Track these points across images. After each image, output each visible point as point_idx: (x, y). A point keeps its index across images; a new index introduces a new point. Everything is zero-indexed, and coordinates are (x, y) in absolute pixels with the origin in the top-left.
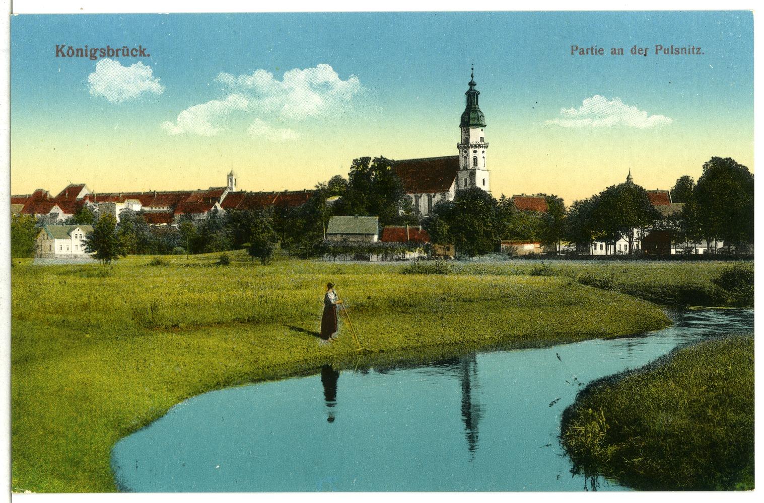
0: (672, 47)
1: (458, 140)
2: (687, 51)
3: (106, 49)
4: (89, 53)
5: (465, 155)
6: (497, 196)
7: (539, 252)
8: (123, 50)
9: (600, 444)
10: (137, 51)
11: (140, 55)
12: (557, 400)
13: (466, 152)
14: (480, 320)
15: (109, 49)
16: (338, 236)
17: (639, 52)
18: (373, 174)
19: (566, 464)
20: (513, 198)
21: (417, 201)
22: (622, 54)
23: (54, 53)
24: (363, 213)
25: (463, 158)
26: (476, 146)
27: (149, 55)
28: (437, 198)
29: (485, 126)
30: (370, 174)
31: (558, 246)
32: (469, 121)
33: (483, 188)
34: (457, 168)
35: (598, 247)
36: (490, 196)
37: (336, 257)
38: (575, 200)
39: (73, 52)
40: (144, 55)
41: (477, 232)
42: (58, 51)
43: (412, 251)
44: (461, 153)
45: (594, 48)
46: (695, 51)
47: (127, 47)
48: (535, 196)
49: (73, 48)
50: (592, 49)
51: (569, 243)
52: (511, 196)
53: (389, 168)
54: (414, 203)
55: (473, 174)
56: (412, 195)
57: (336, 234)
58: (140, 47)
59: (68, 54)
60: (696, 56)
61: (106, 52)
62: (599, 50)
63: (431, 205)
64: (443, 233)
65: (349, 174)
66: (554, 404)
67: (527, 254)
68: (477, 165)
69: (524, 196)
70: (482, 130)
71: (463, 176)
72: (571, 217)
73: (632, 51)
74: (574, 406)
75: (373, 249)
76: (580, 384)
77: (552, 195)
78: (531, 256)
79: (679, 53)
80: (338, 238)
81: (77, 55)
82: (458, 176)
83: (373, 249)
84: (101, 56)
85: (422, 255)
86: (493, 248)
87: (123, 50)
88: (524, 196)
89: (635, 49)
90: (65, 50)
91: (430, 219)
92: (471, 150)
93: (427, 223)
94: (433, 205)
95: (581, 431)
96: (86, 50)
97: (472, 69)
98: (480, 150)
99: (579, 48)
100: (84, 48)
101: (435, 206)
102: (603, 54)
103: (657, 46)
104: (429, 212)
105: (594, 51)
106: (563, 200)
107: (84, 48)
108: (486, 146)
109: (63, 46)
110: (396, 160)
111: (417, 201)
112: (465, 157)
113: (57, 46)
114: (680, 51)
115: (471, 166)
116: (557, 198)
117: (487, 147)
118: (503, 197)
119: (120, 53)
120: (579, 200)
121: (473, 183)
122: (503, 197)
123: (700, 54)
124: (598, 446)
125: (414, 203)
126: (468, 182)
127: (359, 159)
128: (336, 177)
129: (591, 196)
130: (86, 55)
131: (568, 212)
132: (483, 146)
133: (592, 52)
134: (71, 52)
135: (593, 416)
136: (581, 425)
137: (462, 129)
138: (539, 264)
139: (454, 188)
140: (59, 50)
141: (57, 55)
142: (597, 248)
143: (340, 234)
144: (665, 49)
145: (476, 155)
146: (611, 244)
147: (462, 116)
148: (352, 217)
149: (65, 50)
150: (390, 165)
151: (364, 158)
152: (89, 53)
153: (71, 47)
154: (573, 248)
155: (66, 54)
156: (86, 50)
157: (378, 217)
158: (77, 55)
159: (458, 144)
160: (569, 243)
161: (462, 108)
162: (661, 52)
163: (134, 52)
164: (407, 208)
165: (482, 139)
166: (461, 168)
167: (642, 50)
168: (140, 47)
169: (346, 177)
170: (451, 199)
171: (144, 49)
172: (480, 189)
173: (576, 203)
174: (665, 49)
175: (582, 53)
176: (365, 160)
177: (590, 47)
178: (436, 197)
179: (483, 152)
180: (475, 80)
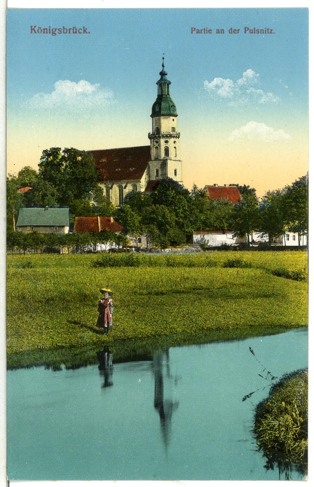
0: (255, 29)
1: (149, 129)
2: (264, 31)
4: (51, 32)
5: (156, 145)
6: (188, 186)
7: (232, 243)
8: (73, 29)
9: (293, 438)
10: (81, 29)
12: (250, 394)
13: (157, 142)
14: (172, 313)
16: (28, 228)
18: (63, 165)
19: (261, 460)
20: (205, 188)
21: (108, 192)
22: (223, 33)
23: (30, 31)
24: (53, 205)
25: (154, 149)
26: (167, 136)
28: (129, 189)
29: (176, 116)
30: (60, 165)
31: (250, 237)
32: (160, 112)
33: (175, 179)
34: (148, 158)
35: (291, 238)
36: (181, 187)
37: (26, 250)
38: (268, 191)
39: (41, 31)
41: (169, 224)
42: (32, 29)
43: (103, 243)
44: (152, 143)
45: (206, 29)
46: (269, 31)
47: (75, 28)
48: (227, 186)
49: (41, 28)
50: (204, 30)
51: (262, 233)
52: (203, 187)
53: (79, 158)
54: (105, 194)
55: (164, 164)
56: (103, 186)
57: (26, 226)
58: (84, 27)
59: (38, 32)
60: (270, 34)
61: (62, 31)
62: (209, 31)
63: (122, 197)
64: (135, 225)
65: (39, 165)
66: (247, 398)
67: (220, 245)
68: (168, 156)
69: (216, 186)
70: (173, 120)
71: (154, 166)
72: (263, 208)
73: (229, 32)
74: (267, 400)
75: (64, 241)
76: (273, 378)
77: (245, 185)
78: (224, 248)
79: (259, 33)
80: (27, 231)
82: (149, 165)
83: (64, 241)
84: (59, 33)
85: (114, 247)
86: (185, 240)
87: (73, 29)
88: (216, 186)
90: (36, 29)
91: (121, 210)
92: (162, 141)
93: (120, 214)
94: (124, 196)
95: (274, 426)
96: (50, 29)
97: (163, 58)
98: (171, 140)
99: (196, 29)
100: (264, 29)
101: (126, 197)
102: (211, 33)
103: (192, 28)
104: (120, 203)
105: (205, 31)
106: (255, 191)
107: (48, 28)
108: (178, 136)
109: (35, 27)
110: (86, 150)
111: (108, 192)
113: (32, 27)
114: (260, 31)
115: (163, 155)
116: (249, 188)
117: (179, 137)
118: (195, 187)
119: (71, 31)
120: (271, 191)
121: (165, 174)
122: (195, 187)
123: (272, 33)
124: (291, 440)
125: (105, 194)
126: (160, 173)
127: (49, 150)
128: (25, 168)
129: (284, 187)
130: (50, 33)
131: (260, 203)
132: (174, 136)
133: (204, 31)
134: (40, 31)
135: (286, 409)
136: (275, 419)
137: (153, 120)
138: (231, 256)
139: (146, 179)
140: (32, 29)
141: (32, 33)
142: (290, 239)
143: (30, 226)
144: (250, 30)
146: (303, 235)
147: (153, 105)
148: (42, 209)
149: (36, 29)
150: (81, 155)
151: (54, 148)
152: (51, 32)
153: (40, 28)
154: (266, 239)
155: (37, 32)
156: (50, 29)
157: (68, 209)
158: (44, 32)
159: (149, 134)
160: (262, 233)
161: (153, 98)
162: (248, 32)
163: (80, 30)
164: (99, 198)
165: (173, 129)
166: (153, 158)
167: (236, 30)
168: (84, 27)
169: (36, 169)
170: (143, 190)
172: (172, 179)
173: (268, 193)
174: (250, 30)
175: (198, 32)
176: (54, 152)
177: (203, 29)
178: (127, 188)
179: (175, 142)
180: (166, 70)
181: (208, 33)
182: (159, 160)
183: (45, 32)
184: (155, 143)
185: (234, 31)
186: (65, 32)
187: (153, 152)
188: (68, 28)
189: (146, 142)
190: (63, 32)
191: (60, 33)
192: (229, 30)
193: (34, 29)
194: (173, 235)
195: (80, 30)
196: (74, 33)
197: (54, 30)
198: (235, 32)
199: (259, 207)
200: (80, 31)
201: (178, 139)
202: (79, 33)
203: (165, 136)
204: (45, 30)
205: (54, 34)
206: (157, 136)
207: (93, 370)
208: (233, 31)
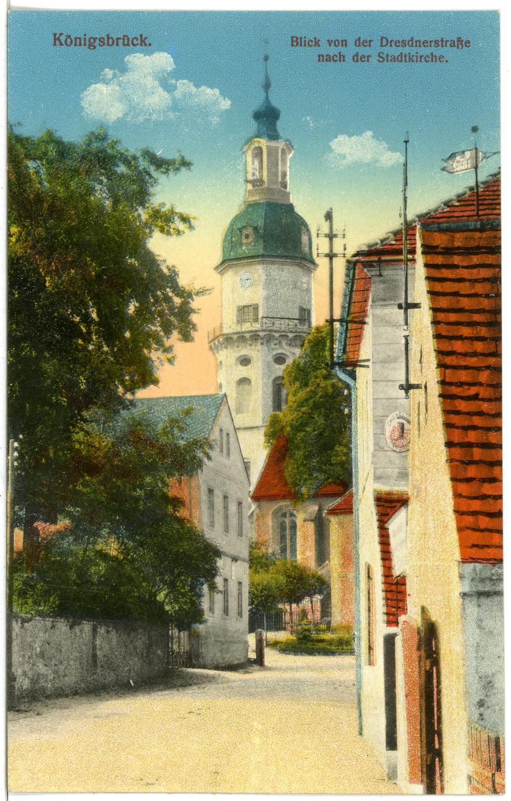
2: (83, 42)
8: (123, 39)
10: (137, 40)
15: (108, 38)
22: (346, 45)
27: (150, 45)
39: (71, 42)
40: (146, 45)
61: (106, 42)
73: (354, 59)
84: (100, 45)
87: (123, 39)
89: (412, 41)
90: (63, 39)
107: (83, 37)
109: (61, 34)
113: (55, 35)
119: (121, 42)
130: (85, 45)
134: (69, 40)
140: (56, 39)
141: (55, 44)
149: (63, 39)
152: (87, 43)
167: (399, 42)
171: (146, 38)
180: (275, 103)
181: (438, 60)
183: (418, 45)
185: (363, 43)
186: (110, 43)
191: (380, 53)
192: (354, 57)
193: (59, 39)
195: (135, 40)
196: (124, 45)
197: (92, 41)
198: (426, 44)
199: (454, 717)
200: (135, 42)
205: (92, 46)
207: (358, 370)
208: (359, 58)
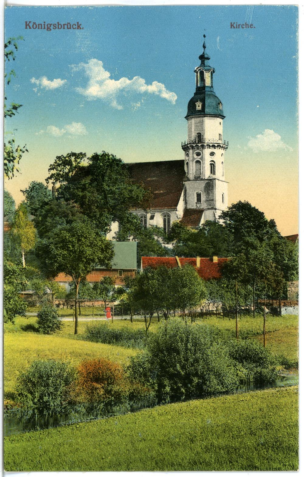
2: (43, 26)
3: (57, 24)
4: (46, 27)
5: (198, 158)
11: (78, 28)
13: (198, 154)
15: (58, 25)
17: (250, 27)
23: (230, 27)
26: (214, 146)
40: (80, 28)
42: (26, 26)
47: (69, 23)
58: (78, 23)
61: (57, 26)
81: (39, 28)
84: (53, 28)
87: (67, 25)
90: (31, 25)
92: (207, 152)
96: (44, 25)
98: (218, 151)
107: (43, 24)
109: (30, 22)
112: (198, 162)
113: (231, 23)
115: (207, 174)
119: (66, 26)
130: (44, 28)
134: (35, 25)
140: (232, 26)
141: (26, 28)
145: (214, 158)
149: (31, 25)
152: (46, 27)
153: (35, 23)
156: (44, 25)
158: (39, 28)
163: (243, 26)
166: (191, 176)
168: (78, 23)
171: (80, 25)
180: (16, 49)
182: (202, 180)
183: (40, 27)
184: (195, 156)
187: (191, 170)
188: (62, 24)
189: (180, 155)
190: (57, 28)
193: (28, 25)
194: (240, 364)
195: (74, 25)
196: (68, 28)
197: (49, 26)
201: (208, 59)
202: (73, 28)
203: (211, 145)
204: (40, 26)
205: (49, 29)
206: (200, 145)
